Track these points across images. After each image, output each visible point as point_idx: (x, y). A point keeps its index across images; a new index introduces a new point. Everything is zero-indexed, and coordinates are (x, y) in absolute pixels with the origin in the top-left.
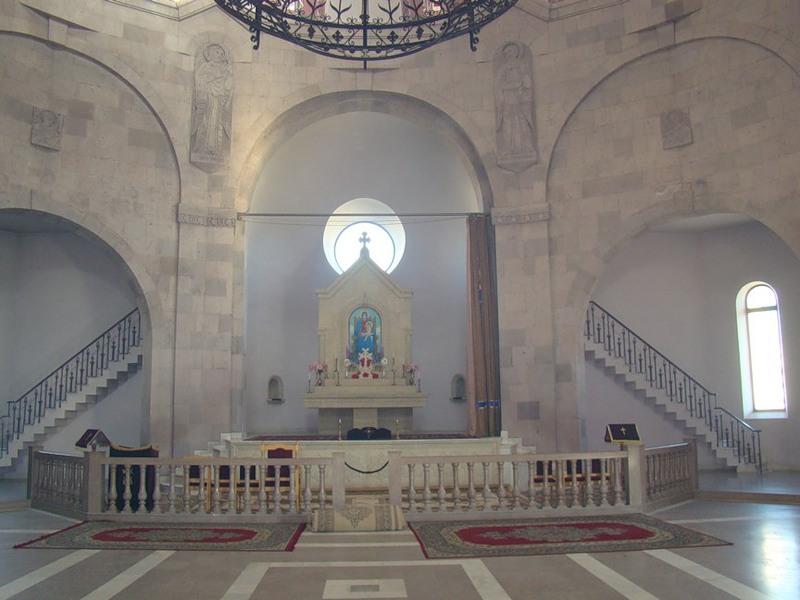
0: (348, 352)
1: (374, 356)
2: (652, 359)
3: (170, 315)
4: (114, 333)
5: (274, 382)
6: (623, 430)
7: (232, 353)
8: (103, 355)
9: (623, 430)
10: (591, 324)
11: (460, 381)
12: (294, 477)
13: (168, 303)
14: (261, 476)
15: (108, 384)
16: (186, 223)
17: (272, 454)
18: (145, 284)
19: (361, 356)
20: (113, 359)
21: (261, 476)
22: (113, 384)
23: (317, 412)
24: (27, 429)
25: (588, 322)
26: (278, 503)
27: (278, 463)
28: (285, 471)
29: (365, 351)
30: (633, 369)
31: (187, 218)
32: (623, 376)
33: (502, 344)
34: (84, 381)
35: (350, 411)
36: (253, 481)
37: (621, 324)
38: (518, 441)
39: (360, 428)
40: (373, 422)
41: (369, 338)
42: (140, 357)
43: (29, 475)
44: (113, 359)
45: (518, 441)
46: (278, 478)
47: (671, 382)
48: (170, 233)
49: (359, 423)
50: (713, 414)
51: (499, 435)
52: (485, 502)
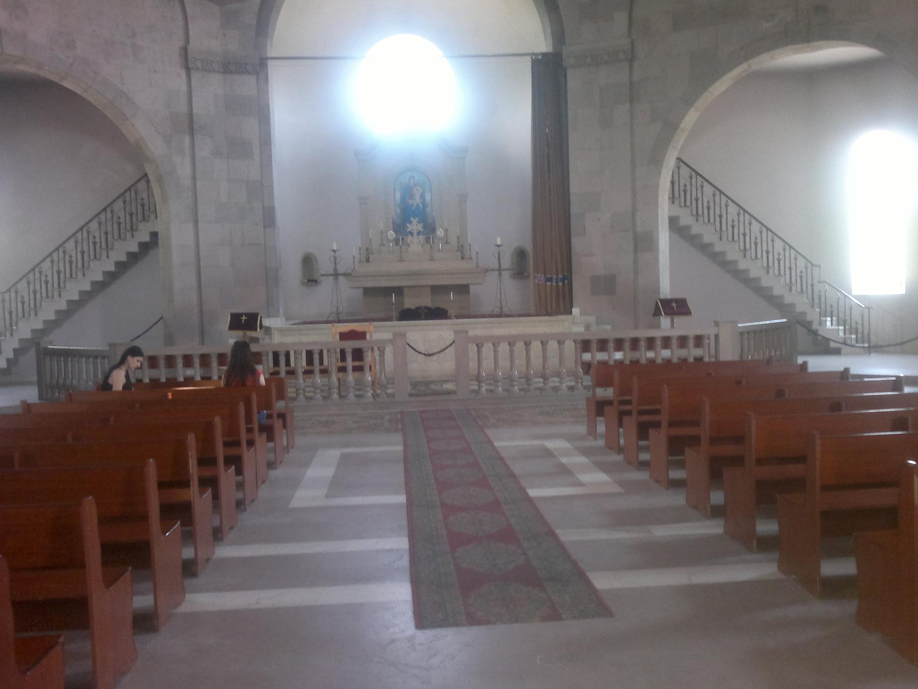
0: (393, 223)
1: (425, 227)
2: (747, 224)
3: (188, 182)
4: (119, 205)
5: (308, 261)
6: (674, 305)
7: (265, 227)
8: (106, 233)
9: (674, 305)
10: (676, 185)
11: (521, 254)
12: (368, 358)
13: (183, 169)
14: (332, 362)
15: (128, 258)
16: (197, 69)
17: (344, 336)
18: (156, 147)
19: (410, 228)
20: (71, 276)
21: (332, 362)
22: (122, 267)
23: (361, 291)
24: (141, 226)
25: (673, 183)
26: (352, 390)
27: (350, 345)
28: (358, 354)
29: (415, 221)
30: (724, 239)
31: (199, 64)
32: (710, 245)
33: (574, 209)
34: (86, 265)
35: (399, 291)
36: (288, 368)
37: (711, 184)
38: (592, 319)
39: (413, 307)
40: (426, 301)
41: (418, 205)
42: (154, 235)
43: (288, 444)
44: (71, 276)
45: (592, 319)
46: (350, 363)
47: (768, 252)
48: (179, 81)
49: (410, 303)
50: (815, 288)
51: (571, 313)
52: (561, 383)
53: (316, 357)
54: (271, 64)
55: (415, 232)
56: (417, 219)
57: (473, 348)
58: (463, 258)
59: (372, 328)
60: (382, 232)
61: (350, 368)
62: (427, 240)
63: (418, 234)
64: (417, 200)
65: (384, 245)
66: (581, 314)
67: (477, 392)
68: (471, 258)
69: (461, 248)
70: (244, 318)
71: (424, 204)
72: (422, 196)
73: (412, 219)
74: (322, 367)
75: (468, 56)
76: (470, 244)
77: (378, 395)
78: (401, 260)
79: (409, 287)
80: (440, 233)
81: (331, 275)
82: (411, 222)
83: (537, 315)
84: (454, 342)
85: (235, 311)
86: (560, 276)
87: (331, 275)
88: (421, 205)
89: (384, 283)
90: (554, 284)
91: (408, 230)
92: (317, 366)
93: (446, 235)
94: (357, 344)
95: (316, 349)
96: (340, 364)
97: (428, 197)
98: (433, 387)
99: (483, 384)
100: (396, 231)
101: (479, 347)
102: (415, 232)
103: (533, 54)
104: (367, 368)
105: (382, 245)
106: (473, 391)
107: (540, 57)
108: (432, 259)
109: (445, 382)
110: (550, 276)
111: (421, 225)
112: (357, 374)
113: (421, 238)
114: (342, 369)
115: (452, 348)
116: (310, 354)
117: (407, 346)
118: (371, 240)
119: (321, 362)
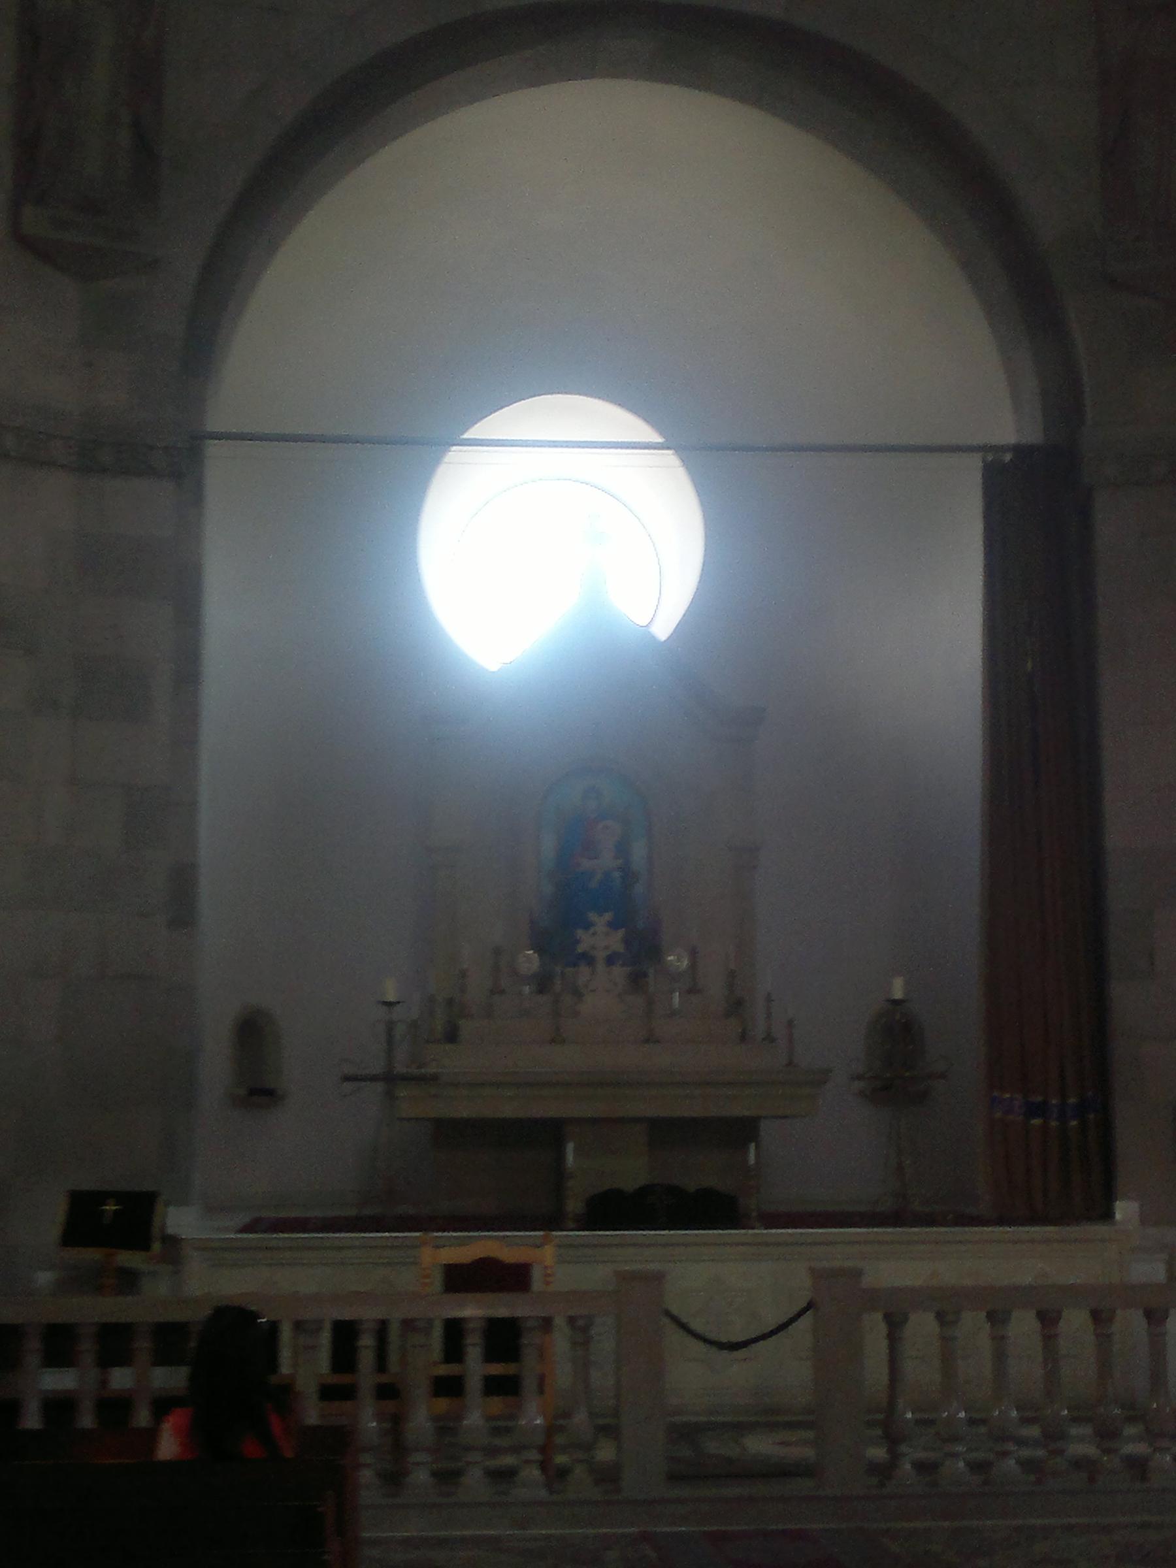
19: (586, 941)
29: (600, 921)
51: (1107, 1215)
53: (366, 1341)
54: (213, 449)
55: (601, 955)
56: (608, 916)
57: (875, 1329)
58: (743, 1037)
59: (548, 1253)
60: (497, 952)
61: (474, 1383)
62: (637, 980)
63: (610, 960)
64: (607, 860)
65: (502, 992)
66: (1144, 1221)
67: (883, 1471)
68: (770, 1038)
69: (736, 1006)
70: (110, 1207)
71: (628, 875)
72: (622, 849)
73: (593, 916)
74: (384, 1379)
75: (773, 449)
76: (769, 999)
77: (563, 1473)
78: (557, 1039)
79: (579, 1121)
80: (676, 960)
81: (374, 1078)
82: (587, 926)
83: (1001, 1221)
84: (810, 1306)
85: (88, 1182)
86: (1072, 1100)
87: (374, 1078)
88: (617, 874)
89: (509, 1109)
90: (1054, 1123)
91: (580, 949)
92: (366, 1375)
93: (693, 966)
94: (502, 1306)
95: (369, 1314)
96: (443, 1370)
97: (639, 852)
98: (713, 1447)
99: (904, 1448)
100: (540, 950)
101: (895, 1324)
102: (601, 955)
103: (984, 449)
104: (529, 1384)
105: (496, 991)
106: (874, 1468)
107: (1008, 457)
108: (650, 1039)
109: (740, 1428)
110: (1040, 1099)
111: (621, 933)
112: (497, 1404)
113: (619, 973)
114: (449, 1387)
115: (805, 1322)
116: (345, 1333)
117: (666, 1321)
118: (463, 974)
119: (381, 1363)
